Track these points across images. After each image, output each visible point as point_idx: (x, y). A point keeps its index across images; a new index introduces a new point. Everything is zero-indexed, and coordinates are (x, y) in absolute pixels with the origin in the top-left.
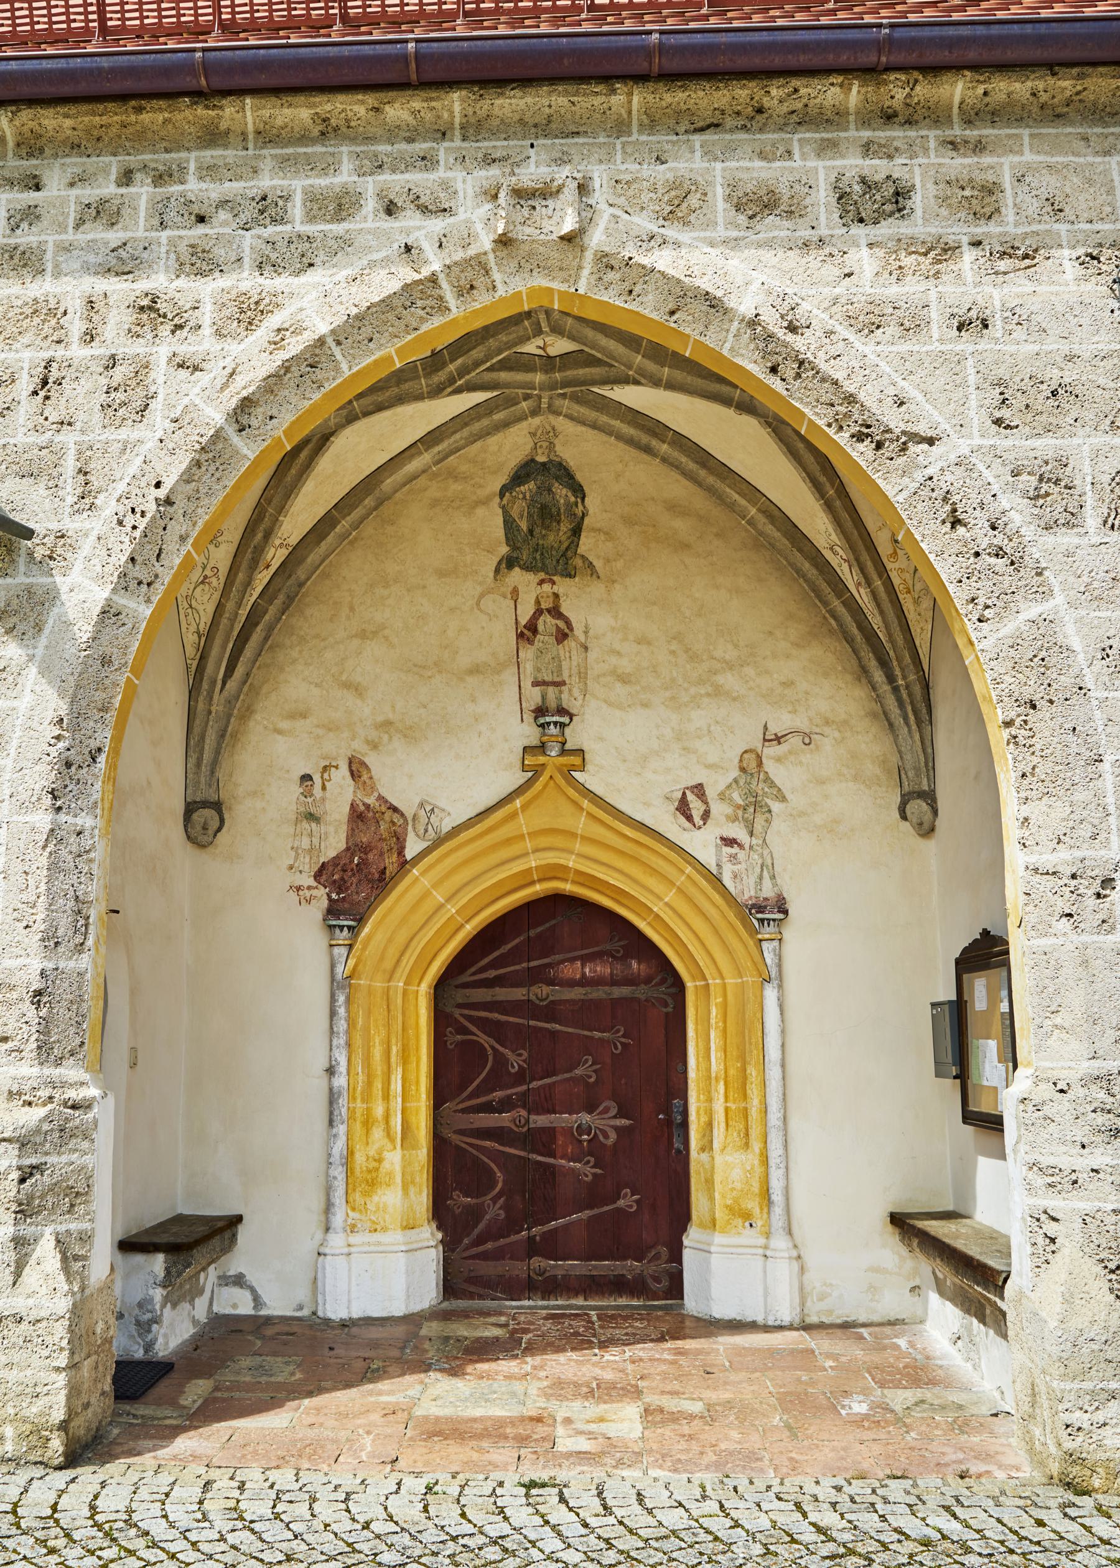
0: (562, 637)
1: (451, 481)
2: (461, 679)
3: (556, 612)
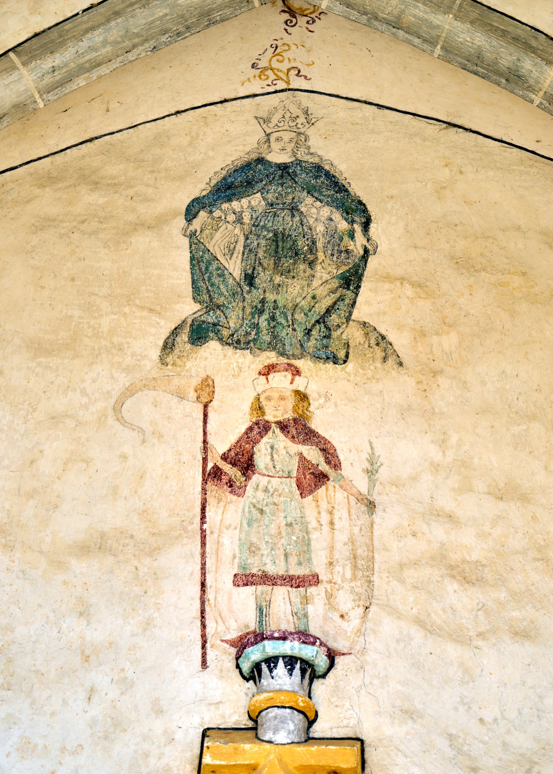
0: (313, 479)
1: (83, 189)
2: (59, 565)
3: (299, 428)
